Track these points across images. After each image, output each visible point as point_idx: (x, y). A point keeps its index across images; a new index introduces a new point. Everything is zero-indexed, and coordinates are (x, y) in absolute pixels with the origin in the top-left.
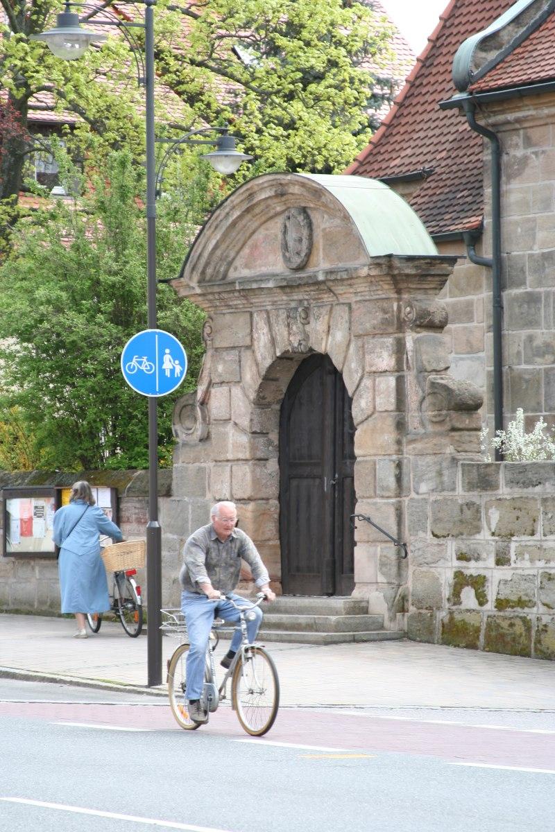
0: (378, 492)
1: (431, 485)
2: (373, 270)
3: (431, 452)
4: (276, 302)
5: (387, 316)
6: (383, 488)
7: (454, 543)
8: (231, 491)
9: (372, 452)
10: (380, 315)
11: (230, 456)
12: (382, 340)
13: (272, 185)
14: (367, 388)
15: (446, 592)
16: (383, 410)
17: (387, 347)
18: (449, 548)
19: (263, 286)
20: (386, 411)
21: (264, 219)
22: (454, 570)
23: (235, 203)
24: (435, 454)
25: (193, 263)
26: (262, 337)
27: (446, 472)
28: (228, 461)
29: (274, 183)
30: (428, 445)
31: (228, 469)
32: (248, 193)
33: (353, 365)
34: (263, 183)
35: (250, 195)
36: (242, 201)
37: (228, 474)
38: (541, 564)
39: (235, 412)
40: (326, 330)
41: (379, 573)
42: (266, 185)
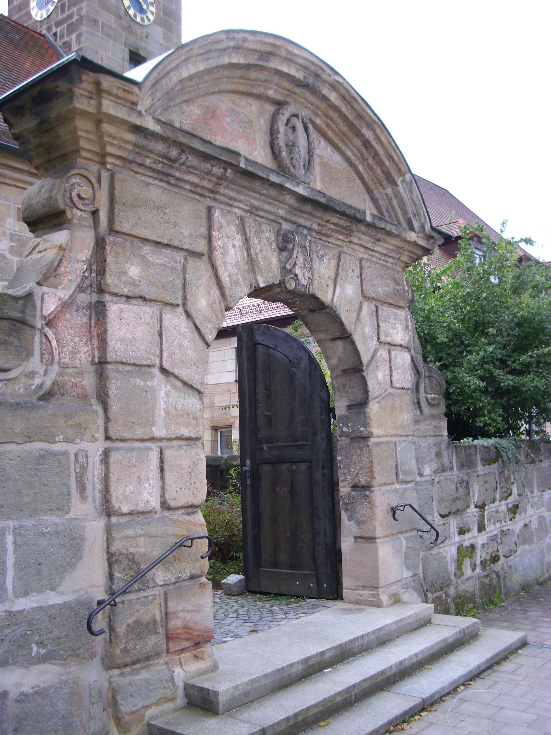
0: (401, 477)
1: (435, 466)
2: (421, 239)
3: (433, 434)
4: (257, 209)
5: (397, 288)
6: (406, 473)
7: (455, 521)
8: (163, 496)
9: (392, 432)
10: (392, 285)
11: (159, 431)
12: (396, 311)
13: (306, 68)
14: (384, 359)
15: (452, 568)
16: (401, 386)
17: (401, 320)
18: (451, 526)
19: (288, 185)
20: (403, 388)
21: (242, 88)
22: (457, 545)
23: (246, 45)
24: (435, 436)
25: (166, 70)
26: (232, 251)
27: (445, 453)
28: (153, 439)
29: (313, 68)
30: (430, 427)
31: (154, 455)
32: (269, 49)
33: (367, 330)
34: (299, 56)
35: (270, 53)
36: (254, 50)
37: (154, 463)
38: (498, 525)
39: (170, 356)
40: (333, 277)
41: (404, 568)
42: (300, 61)
